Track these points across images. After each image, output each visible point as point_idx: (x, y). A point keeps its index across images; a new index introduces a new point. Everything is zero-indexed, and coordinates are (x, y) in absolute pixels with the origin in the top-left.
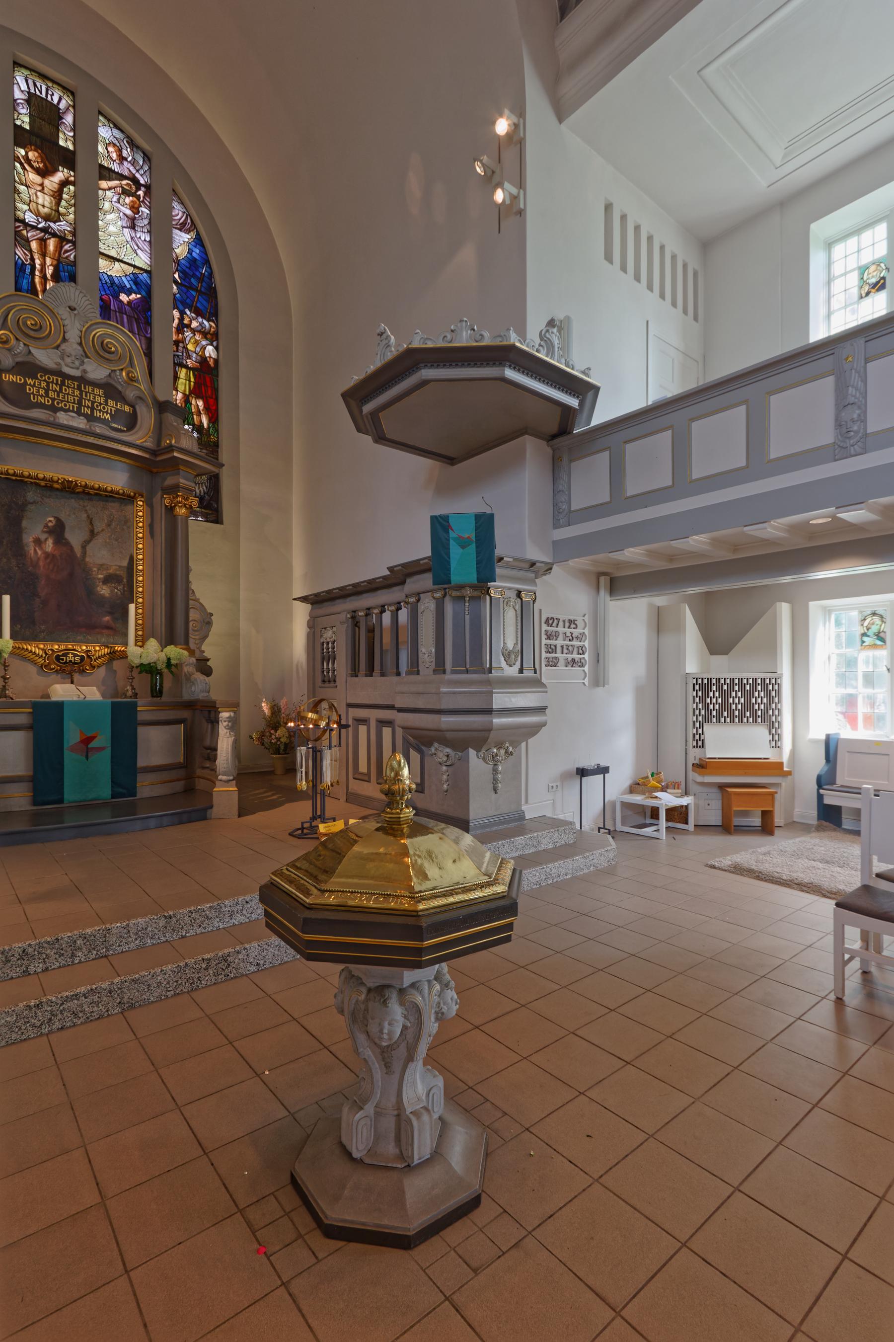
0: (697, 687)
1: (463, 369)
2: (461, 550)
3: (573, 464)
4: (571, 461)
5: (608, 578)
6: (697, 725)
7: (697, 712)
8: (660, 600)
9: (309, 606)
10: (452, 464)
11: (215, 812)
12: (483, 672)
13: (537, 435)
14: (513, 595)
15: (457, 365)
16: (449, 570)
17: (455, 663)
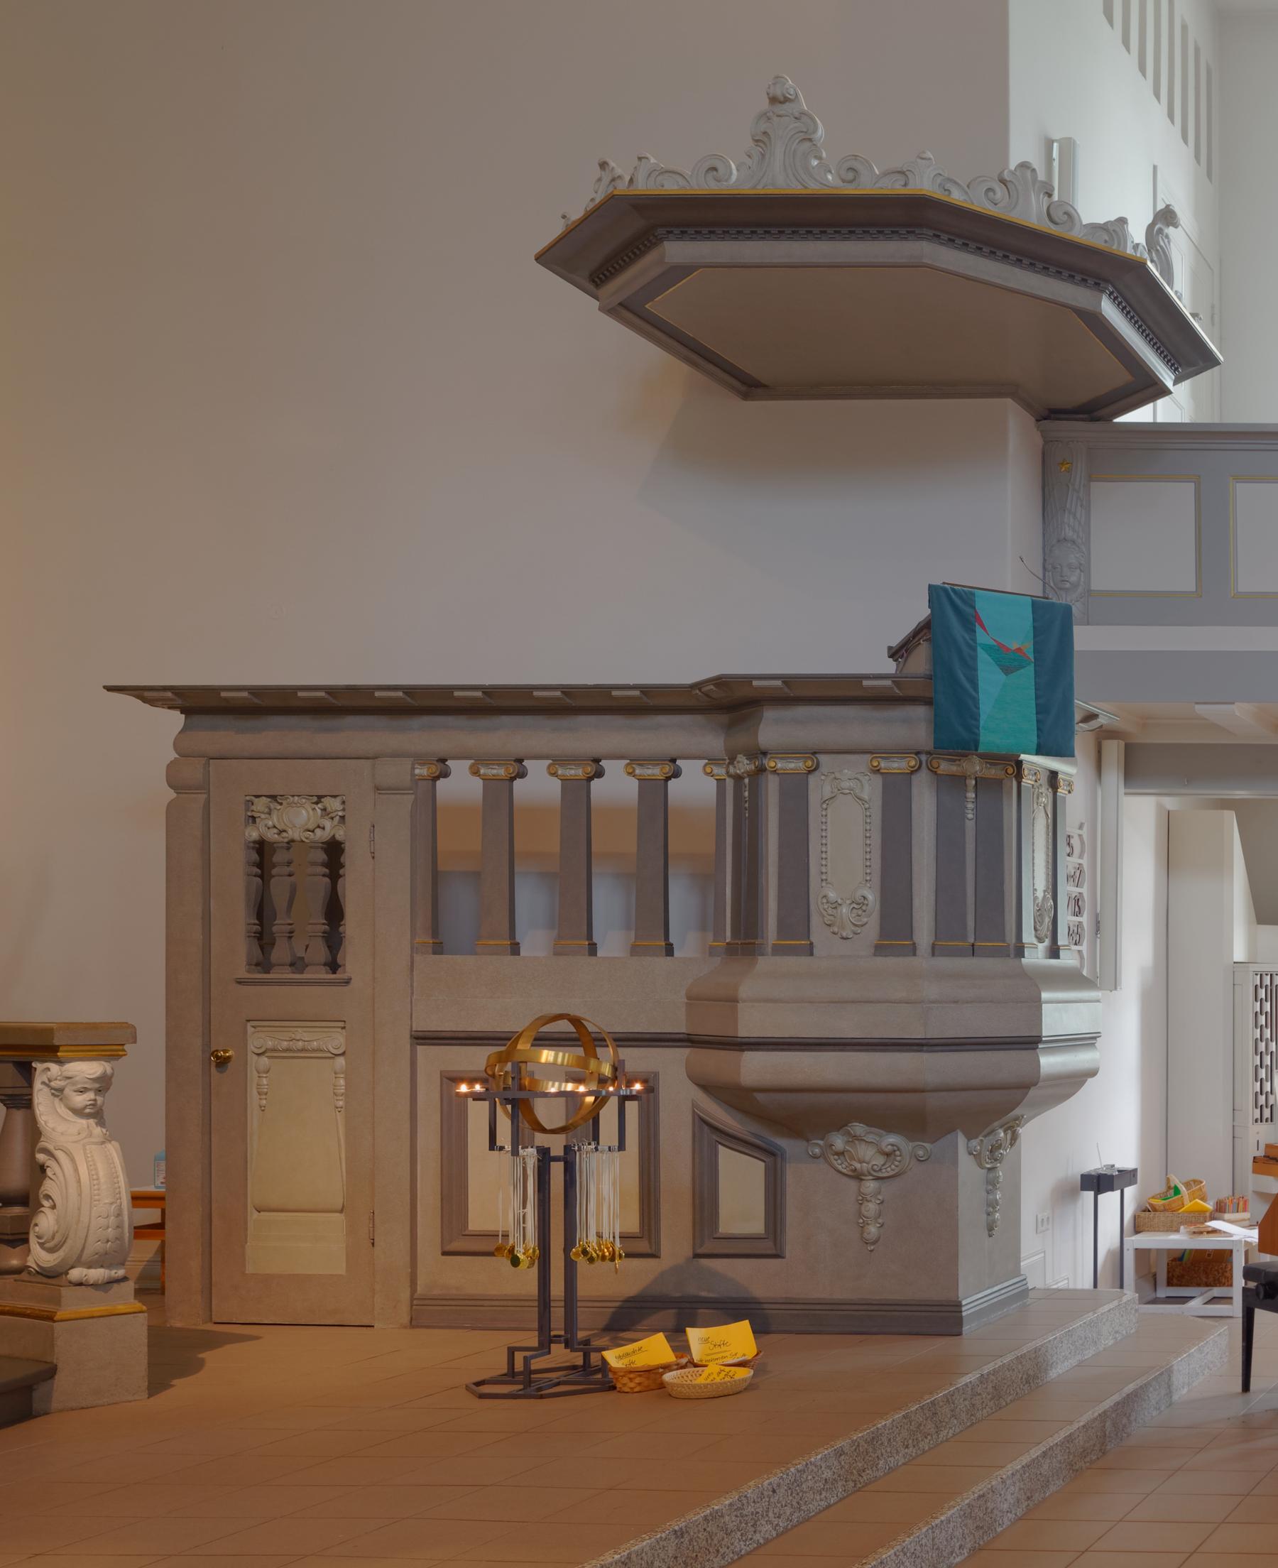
0: (1262, 994)
1: (1017, 270)
2: (1002, 677)
3: (1097, 488)
4: (1090, 479)
5: (1122, 743)
6: (1262, 1073)
7: (1262, 1046)
8: (1170, 803)
9: (176, 719)
10: (746, 396)
11: (63, 1388)
12: (1001, 952)
13: (1027, 405)
14: (1044, 779)
15: (1006, 257)
16: (976, 718)
17: (784, 928)
